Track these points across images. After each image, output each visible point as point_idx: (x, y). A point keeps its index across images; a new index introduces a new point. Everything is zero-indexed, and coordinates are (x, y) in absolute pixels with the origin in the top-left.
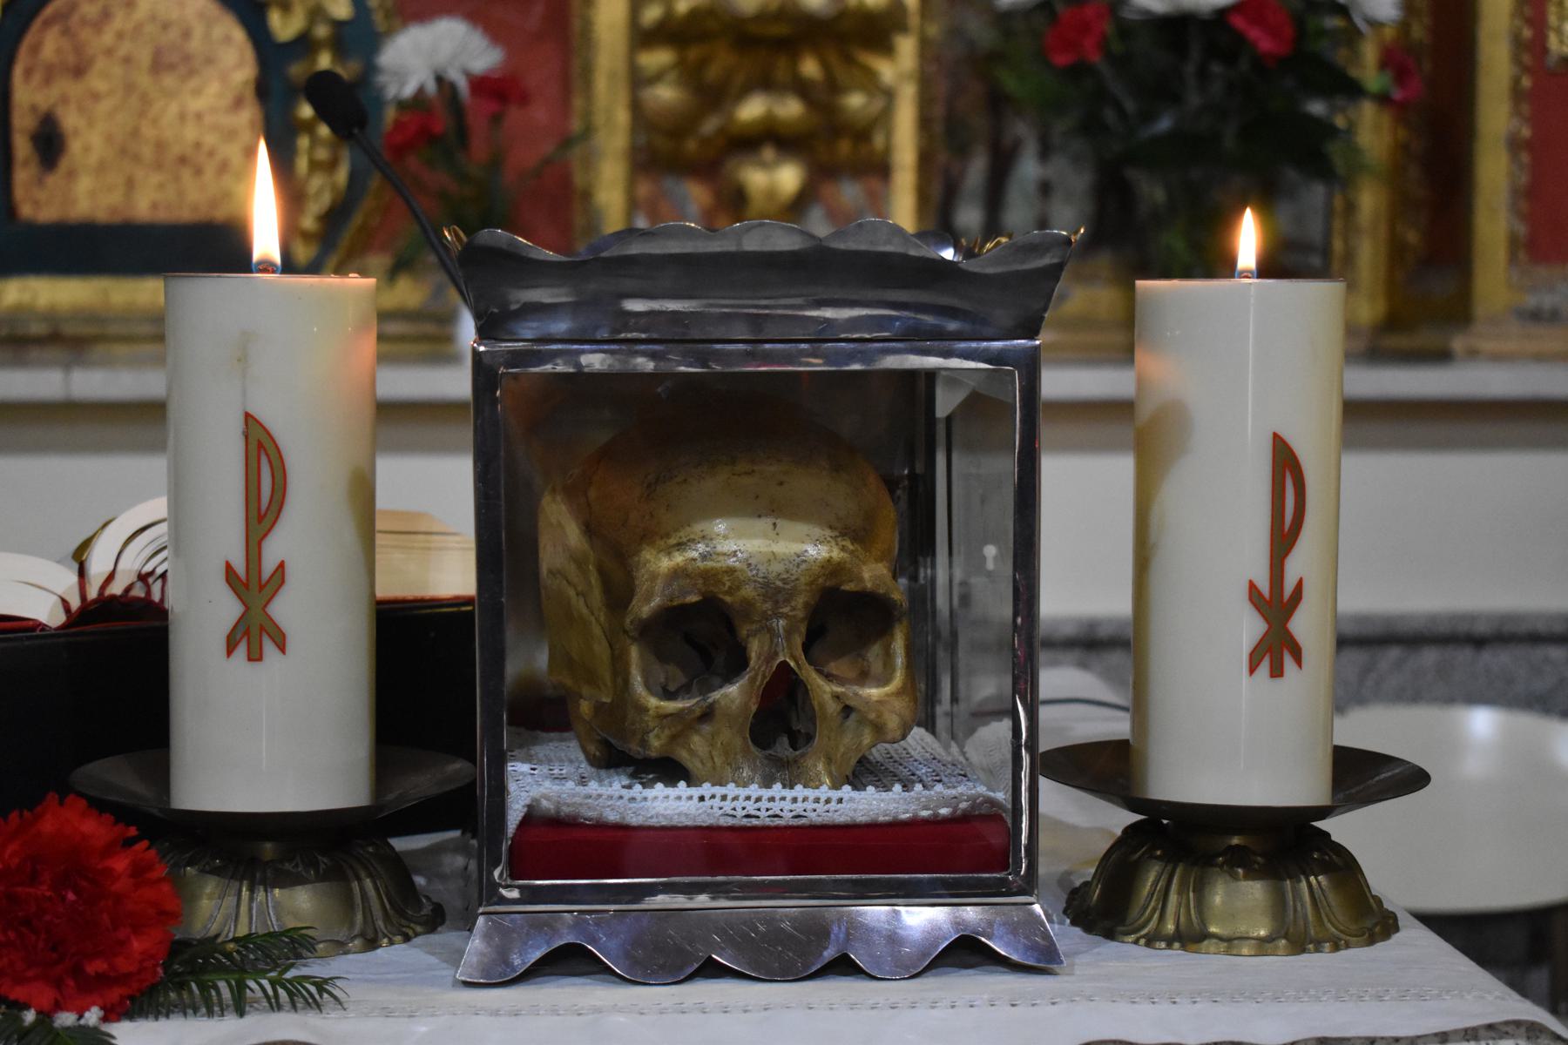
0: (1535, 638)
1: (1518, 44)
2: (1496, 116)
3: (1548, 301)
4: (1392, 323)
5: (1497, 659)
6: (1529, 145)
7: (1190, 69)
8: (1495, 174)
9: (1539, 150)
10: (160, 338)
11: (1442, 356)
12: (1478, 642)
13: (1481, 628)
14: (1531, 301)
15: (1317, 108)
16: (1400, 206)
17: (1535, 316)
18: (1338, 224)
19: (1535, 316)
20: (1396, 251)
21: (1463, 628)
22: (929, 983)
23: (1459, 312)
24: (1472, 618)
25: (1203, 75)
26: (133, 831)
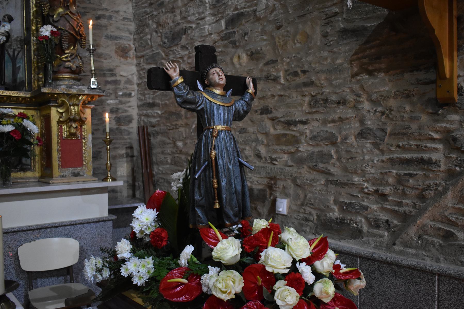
0: (65, 226)
1: (58, 135)
2: (55, 146)
3: (65, 174)
4: (42, 177)
5: (59, 229)
6: (60, 150)
7: (4, 141)
8: (55, 155)
9: (62, 151)
10: (3, 233)
11: (48, 184)
12: (56, 227)
13: (56, 225)
14: (62, 174)
15: (25, 146)
16: (42, 158)
17: (63, 176)
18: (32, 161)
19: (63, 176)
20: (42, 165)
21: (54, 225)
22: (5, 255)
23: (51, 176)
24: (55, 223)
25: (6, 141)
26: (457, 108)
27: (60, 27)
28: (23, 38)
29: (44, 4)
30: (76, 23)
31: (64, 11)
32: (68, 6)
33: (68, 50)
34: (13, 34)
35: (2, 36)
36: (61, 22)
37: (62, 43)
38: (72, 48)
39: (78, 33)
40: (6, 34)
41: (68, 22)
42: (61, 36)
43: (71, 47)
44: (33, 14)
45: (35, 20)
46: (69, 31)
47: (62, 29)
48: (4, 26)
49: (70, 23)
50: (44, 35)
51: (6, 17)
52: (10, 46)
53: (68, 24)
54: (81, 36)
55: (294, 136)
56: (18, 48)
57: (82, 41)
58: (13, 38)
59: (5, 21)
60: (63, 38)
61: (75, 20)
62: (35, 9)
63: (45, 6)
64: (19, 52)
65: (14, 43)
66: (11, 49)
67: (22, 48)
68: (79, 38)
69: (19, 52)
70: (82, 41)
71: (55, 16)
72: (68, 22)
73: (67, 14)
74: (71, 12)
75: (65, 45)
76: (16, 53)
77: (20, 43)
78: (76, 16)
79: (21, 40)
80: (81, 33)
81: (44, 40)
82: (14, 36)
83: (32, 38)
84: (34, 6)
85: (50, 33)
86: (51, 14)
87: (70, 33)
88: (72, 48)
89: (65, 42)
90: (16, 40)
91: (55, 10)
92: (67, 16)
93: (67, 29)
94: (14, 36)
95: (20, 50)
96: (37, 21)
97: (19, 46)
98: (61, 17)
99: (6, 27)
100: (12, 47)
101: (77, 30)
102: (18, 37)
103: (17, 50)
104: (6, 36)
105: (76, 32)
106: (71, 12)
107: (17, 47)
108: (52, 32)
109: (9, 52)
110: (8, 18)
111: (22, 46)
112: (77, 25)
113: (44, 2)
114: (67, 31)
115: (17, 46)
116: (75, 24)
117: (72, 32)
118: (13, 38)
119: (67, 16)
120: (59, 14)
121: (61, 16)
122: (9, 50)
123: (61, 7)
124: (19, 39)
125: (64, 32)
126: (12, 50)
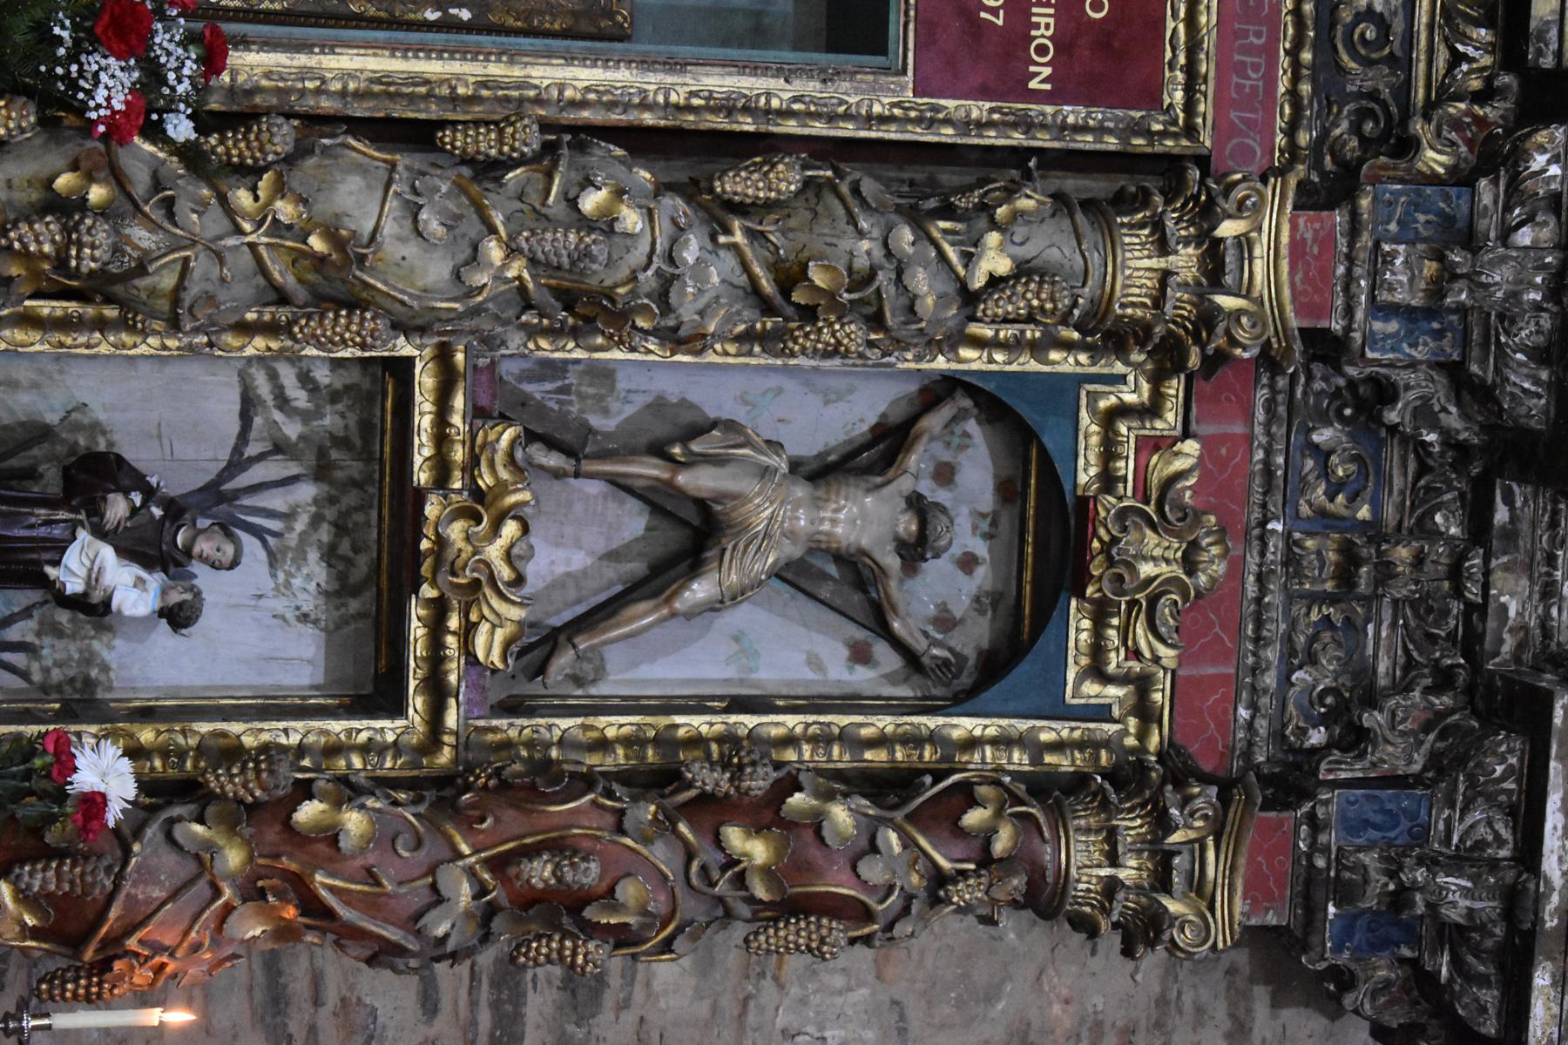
27: (136, 848)
28: (100, 694)
29: (258, 771)
30: (168, 940)
31: (231, 877)
32: (261, 894)
33: (16, 900)
34: (118, 642)
35: (83, 573)
36: (168, 860)
37: (50, 859)
38: (30, 921)
39: (113, 948)
40: (97, 596)
41: (173, 896)
42: (78, 857)
43: (33, 913)
44: (224, 734)
45: (193, 742)
46: (121, 897)
47: (125, 863)
48: (139, 583)
49: (164, 903)
50: (80, 762)
51: (188, 596)
52: (57, 631)
53: (158, 893)
54: (103, 966)
55: (1373, 380)
56: (46, 671)
57: (76, 980)
58: (96, 645)
59: (164, 592)
60: (73, 866)
61: (186, 933)
62: (248, 741)
63: (251, 775)
64: (24, 675)
65: (73, 649)
66: (39, 634)
67: (45, 688)
68: (89, 954)
69: (24, 675)
70: (76, 980)
71: (198, 828)
72: (173, 896)
73: (217, 892)
74: (228, 909)
75: (40, 878)
76: (18, 659)
77: (72, 680)
78: (217, 942)
79: (89, 684)
80: (118, 966)
81: (49, 759)
82: (110, 647)
83: (93, 729)
84: (265, 737)
85: (87, 789)
86: (211, 810)
87: (110, 898)
88: (30, 921)
89: (51, 874)
90: (89, 659)
91: (231, 826)
92: (202, 887)
93: (127, 887)
94: (110, 647)
95: (37, 677)
96: (182, 754)
97: (56, 675)
98: (197, 857)
99: (134, 594)
100: (47, 641)
101: (132, 943)
102: (105, 668)
103: (35, 666)
104: (85, 594)
105: (113, 944)
106: (228, 909)
107: (49, 663)
108: (95, 802)
109: (21, 624)
110: (181, 605)
111: (59, 688)
112: (158, 948)
113: (271, 772)
114: (117, 887)
115: (58, 664)
116: (162, 930)
117: (114, 913)
118: (96, 645)
119: (202, 887)
120: (211, 848)
121: (202, 860)
122: (32, 624)
123: (250, 858)
124: (94, 673)
125: (108, 869)
126: (30, 638)
